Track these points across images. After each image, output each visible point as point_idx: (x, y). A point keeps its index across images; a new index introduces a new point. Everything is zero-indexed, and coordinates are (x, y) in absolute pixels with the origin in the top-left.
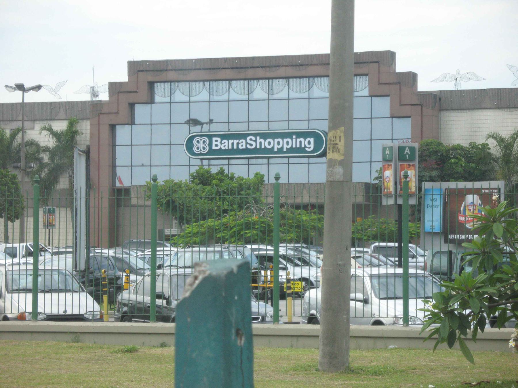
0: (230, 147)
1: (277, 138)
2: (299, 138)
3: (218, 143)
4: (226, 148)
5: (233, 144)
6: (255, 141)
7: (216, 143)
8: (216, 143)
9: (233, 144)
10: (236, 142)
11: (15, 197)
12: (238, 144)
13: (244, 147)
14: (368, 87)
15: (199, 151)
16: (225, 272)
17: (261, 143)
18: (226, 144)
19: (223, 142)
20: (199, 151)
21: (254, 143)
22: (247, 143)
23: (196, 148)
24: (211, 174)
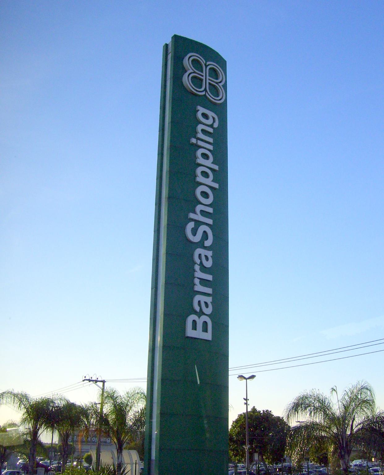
0: (209, 291)
1: (196, 157)
2: (196, 133)
3: (199, 322)
4: (209, 300)
5: (203, 282)
6: (198, 223)
7: (200, 326)
8: (200, 326)
9: (203, 282)
10: (199, 274)
11: (325, 469)
12: (203, 269)
13: (210, 254)
14: (154, 288)
15: (203, 91)
16: (62, 404)
17: (203, 213)
18: (203, 299)
19: (197, 308)
20: (203, 91)
21: (202, 228)
22: (201, 245)
23: (191, 59)
24: (338, 419)
